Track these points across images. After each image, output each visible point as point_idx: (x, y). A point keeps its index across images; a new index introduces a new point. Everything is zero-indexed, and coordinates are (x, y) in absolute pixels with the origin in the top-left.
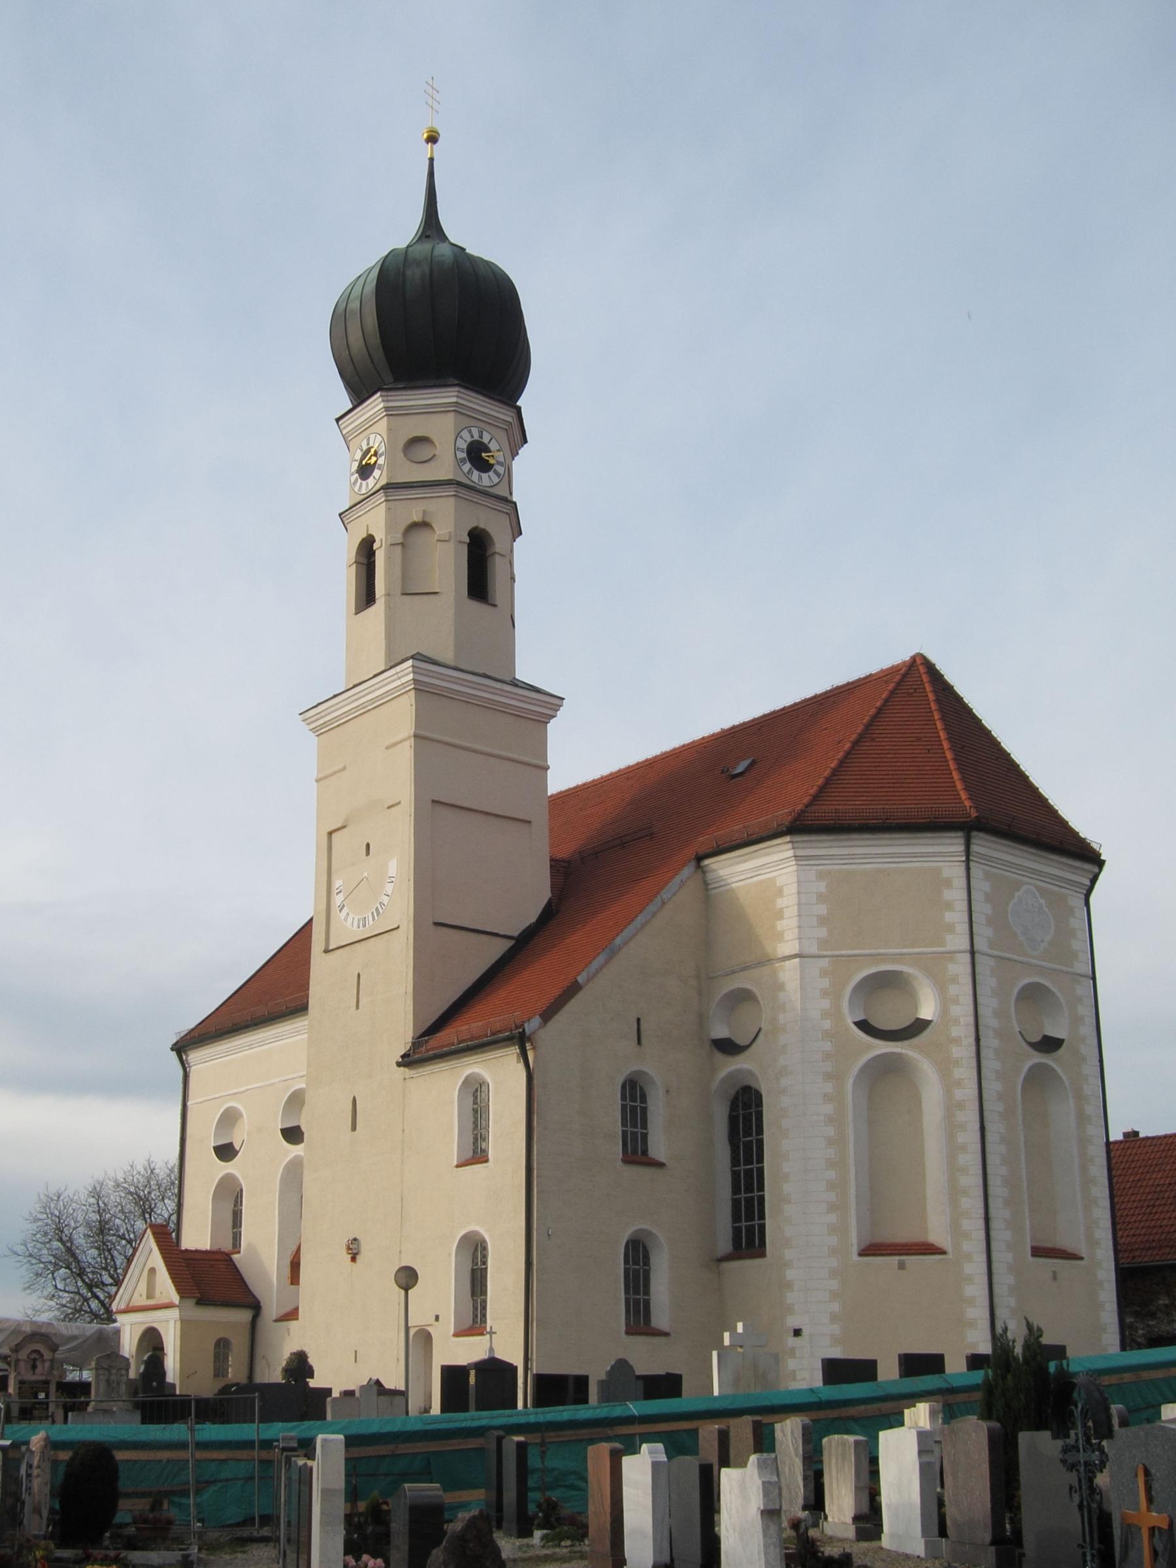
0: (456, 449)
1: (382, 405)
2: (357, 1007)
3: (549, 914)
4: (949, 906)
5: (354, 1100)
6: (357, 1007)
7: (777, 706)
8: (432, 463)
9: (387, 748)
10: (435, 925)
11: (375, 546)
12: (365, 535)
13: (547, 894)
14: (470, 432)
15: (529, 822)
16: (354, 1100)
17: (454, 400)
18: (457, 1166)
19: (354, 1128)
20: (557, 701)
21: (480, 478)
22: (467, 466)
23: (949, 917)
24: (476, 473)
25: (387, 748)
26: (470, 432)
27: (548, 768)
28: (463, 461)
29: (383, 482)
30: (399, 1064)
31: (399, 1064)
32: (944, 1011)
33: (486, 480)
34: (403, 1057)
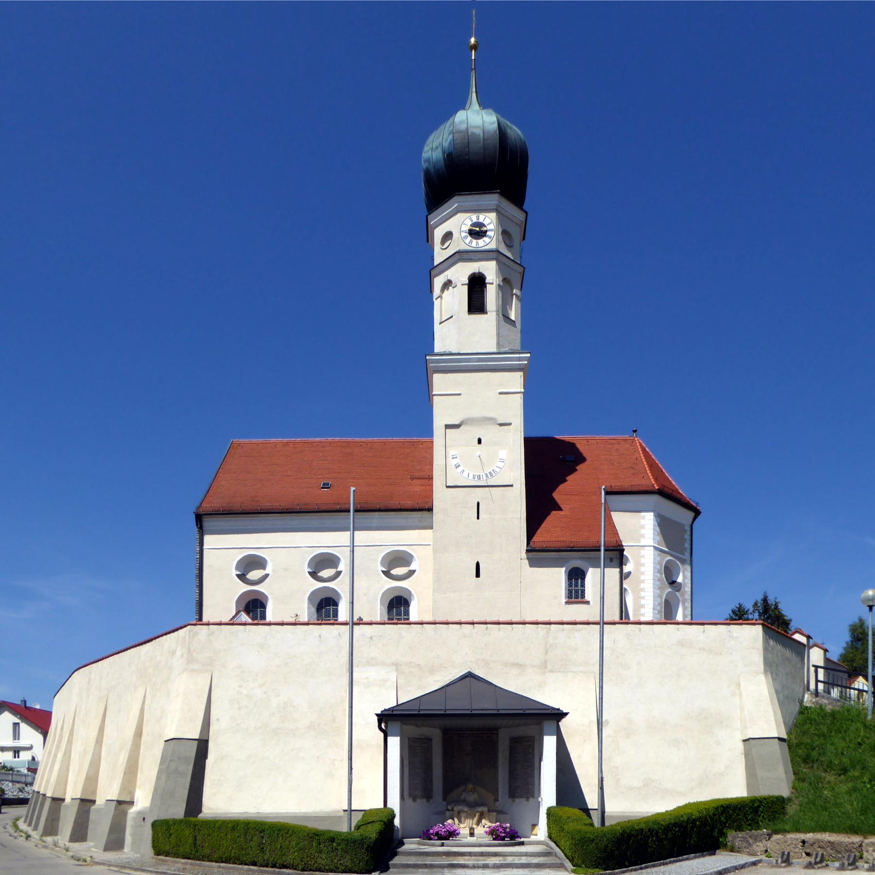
5: (478, 565)
9: (500, 393)
16: (478, 565)
32: (684, 580)
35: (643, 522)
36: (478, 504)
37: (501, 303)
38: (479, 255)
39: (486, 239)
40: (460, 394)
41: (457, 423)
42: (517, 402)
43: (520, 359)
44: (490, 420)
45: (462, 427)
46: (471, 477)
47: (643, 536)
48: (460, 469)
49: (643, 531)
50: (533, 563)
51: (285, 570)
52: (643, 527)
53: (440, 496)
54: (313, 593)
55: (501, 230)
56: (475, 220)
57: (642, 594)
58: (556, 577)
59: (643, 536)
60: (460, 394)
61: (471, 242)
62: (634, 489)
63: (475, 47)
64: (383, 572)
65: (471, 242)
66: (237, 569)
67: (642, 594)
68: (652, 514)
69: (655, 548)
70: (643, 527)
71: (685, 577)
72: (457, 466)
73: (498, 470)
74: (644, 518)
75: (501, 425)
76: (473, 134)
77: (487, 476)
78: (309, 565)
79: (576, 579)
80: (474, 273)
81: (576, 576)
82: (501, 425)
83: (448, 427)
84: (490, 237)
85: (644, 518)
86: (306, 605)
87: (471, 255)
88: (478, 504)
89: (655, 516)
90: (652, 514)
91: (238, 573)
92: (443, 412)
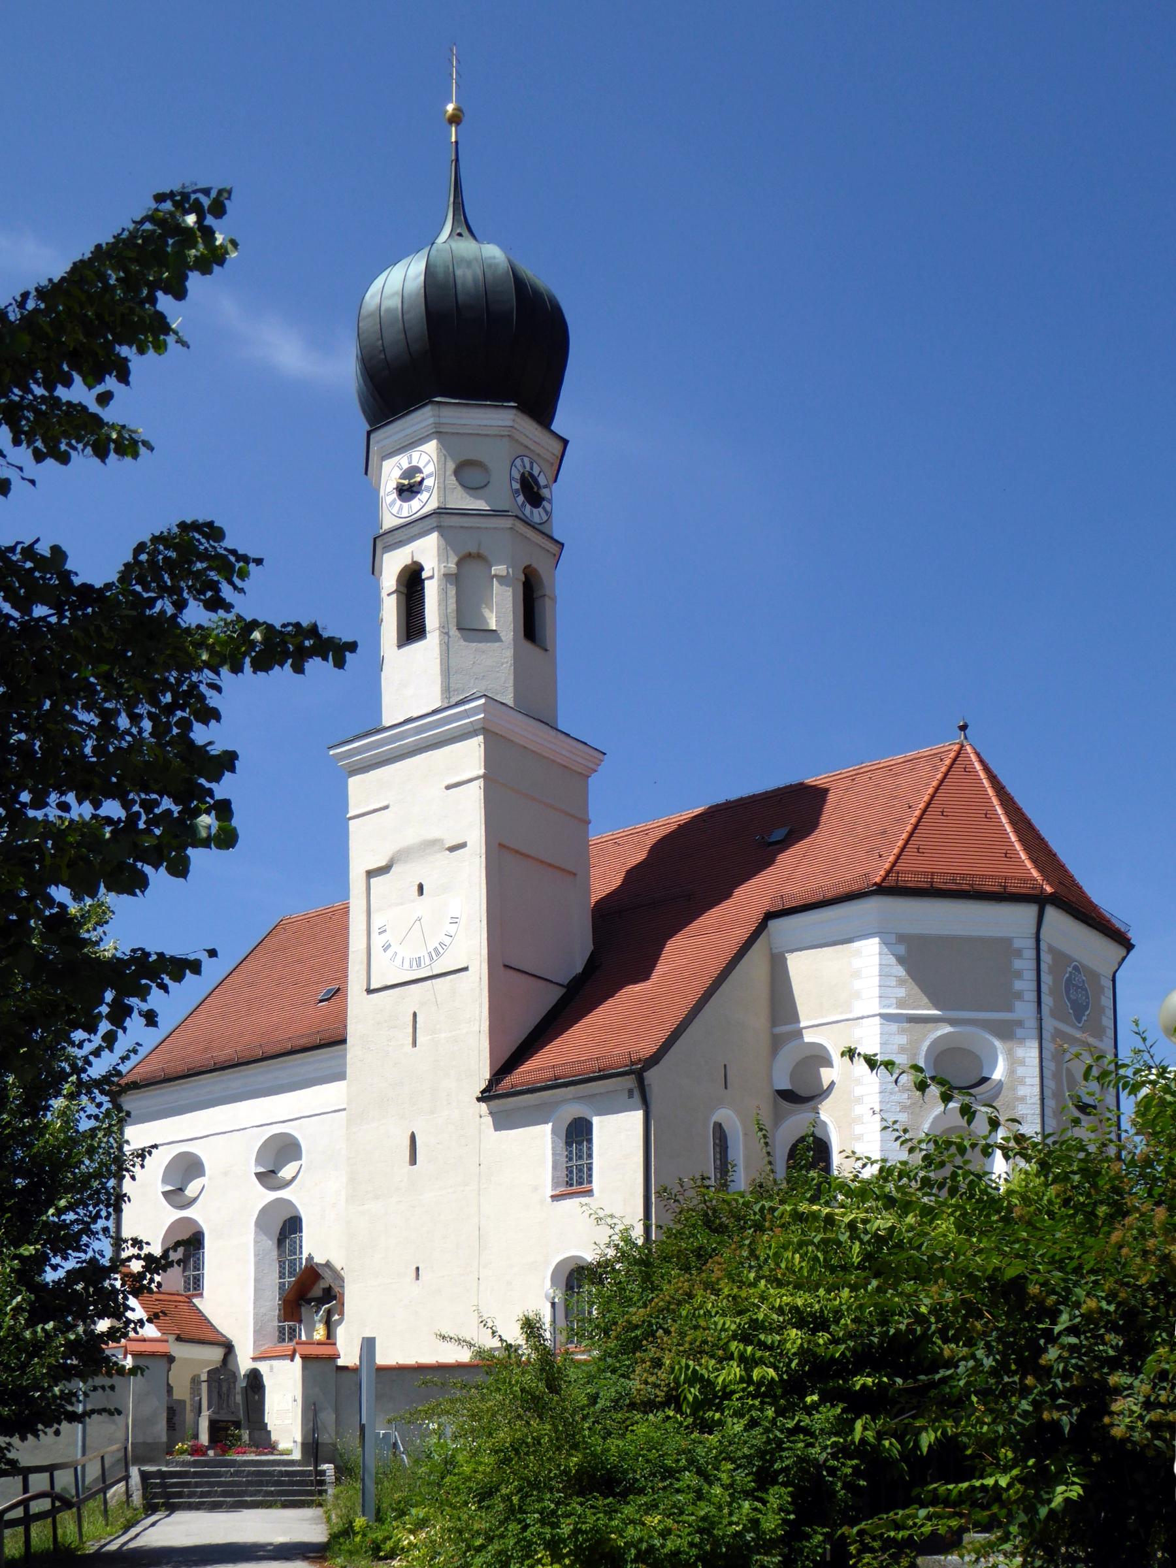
0: (511, 478)
1: (431, 420)
2: (414, 1044)
3: (592, 965)
4: (1019, 975)
5: (413, 1138)
6: (414, 1044)
7: (734, 796)
8: (490, 486)
9: (448, 788)
10: (504, 967)
11: (424, 575)
12: (409, 562)
13: (590, 947)
14: (522, 461)
15: (575, 874)
16: (413, 1138)
17: (510, 423)
18: (555, 1198)
19: (413, 1160)
20: (601, 756)
21: (532, 513)
22: (521, 499)
23: (1018, 985)
24: (528, 507)
25: (448, 788)
26: (522, 461)
27: (589, 822)
28: (517, 491)
29: (433, 505)
30: (479, 1099)
31: (479, 1099)
32: (1011, 1072)
33: (537, 515)
34: (482, 1092)
35: (857, 963)
36: (415, 1015)
37: (452, 606)
38: (415, 529)
39: (424, 496)
40: (386, 807)
41: (383, 863)
42: (473, 798)
43: (467, 714)
44: (431, 845)
45: (393, 869)
46: (407, 965)
47: (857, 995)
48: (390, 952)
49: (857, 984)
50: (502, 1122)
51: (226, 1174)
52: (856, 974)
53: (361, 1013)
54: (265, 1212)
55: (451, 466)
56: (405, 465)
57: (858, 1129)
58: (538, 1142)
59: (857, 995)
60: (386, 807)
61: (401, 508)
62: (829, 895)
63: (455, 119)
64: (165, 1194)
65: (401, 508)
66: (165, 1180)
67: (858, 1129)
68: (876, 940)
69: (885, 1017)
70: (856, 974)
71: (1013, 1063)
72: (386, 948)
73: (447, 940)
74: (858, 953)
75: (452, 849)
76: (388, 310)
77: (431, 958)
78: (259, 1161)
79: (579, 1143)
80: (406, 566)
81: (578, 1135)
82: (452, 849)
83: (370, 874)
84: (428, 489)
85: (858, 953)
86: (251, 1236)
87: (399, 536)
88: (415, 1015)
89: (885, 943)
90: (876, 940)
91: (262, 1170)
92: (365, 847)
